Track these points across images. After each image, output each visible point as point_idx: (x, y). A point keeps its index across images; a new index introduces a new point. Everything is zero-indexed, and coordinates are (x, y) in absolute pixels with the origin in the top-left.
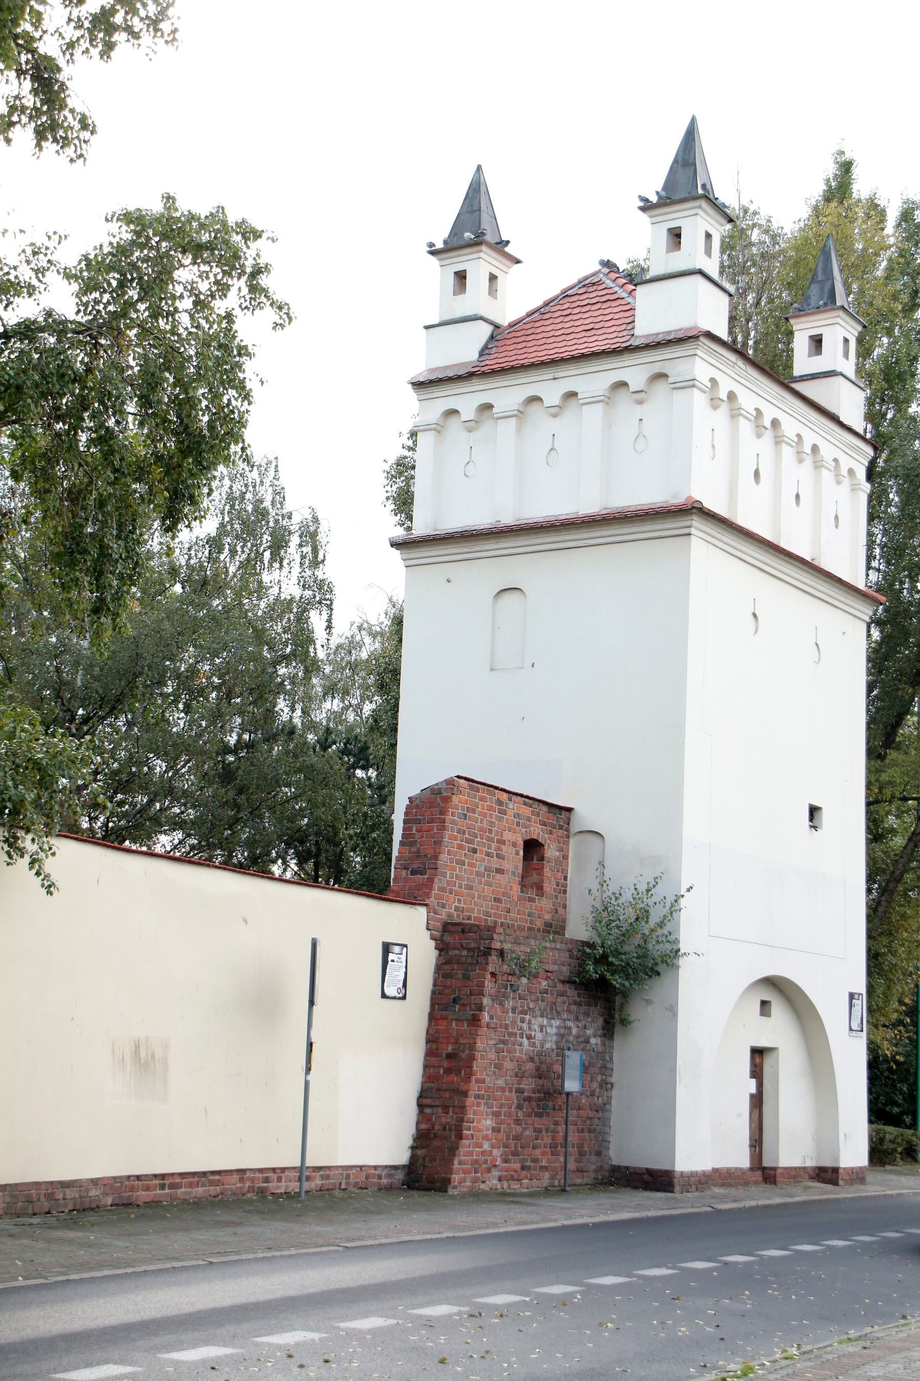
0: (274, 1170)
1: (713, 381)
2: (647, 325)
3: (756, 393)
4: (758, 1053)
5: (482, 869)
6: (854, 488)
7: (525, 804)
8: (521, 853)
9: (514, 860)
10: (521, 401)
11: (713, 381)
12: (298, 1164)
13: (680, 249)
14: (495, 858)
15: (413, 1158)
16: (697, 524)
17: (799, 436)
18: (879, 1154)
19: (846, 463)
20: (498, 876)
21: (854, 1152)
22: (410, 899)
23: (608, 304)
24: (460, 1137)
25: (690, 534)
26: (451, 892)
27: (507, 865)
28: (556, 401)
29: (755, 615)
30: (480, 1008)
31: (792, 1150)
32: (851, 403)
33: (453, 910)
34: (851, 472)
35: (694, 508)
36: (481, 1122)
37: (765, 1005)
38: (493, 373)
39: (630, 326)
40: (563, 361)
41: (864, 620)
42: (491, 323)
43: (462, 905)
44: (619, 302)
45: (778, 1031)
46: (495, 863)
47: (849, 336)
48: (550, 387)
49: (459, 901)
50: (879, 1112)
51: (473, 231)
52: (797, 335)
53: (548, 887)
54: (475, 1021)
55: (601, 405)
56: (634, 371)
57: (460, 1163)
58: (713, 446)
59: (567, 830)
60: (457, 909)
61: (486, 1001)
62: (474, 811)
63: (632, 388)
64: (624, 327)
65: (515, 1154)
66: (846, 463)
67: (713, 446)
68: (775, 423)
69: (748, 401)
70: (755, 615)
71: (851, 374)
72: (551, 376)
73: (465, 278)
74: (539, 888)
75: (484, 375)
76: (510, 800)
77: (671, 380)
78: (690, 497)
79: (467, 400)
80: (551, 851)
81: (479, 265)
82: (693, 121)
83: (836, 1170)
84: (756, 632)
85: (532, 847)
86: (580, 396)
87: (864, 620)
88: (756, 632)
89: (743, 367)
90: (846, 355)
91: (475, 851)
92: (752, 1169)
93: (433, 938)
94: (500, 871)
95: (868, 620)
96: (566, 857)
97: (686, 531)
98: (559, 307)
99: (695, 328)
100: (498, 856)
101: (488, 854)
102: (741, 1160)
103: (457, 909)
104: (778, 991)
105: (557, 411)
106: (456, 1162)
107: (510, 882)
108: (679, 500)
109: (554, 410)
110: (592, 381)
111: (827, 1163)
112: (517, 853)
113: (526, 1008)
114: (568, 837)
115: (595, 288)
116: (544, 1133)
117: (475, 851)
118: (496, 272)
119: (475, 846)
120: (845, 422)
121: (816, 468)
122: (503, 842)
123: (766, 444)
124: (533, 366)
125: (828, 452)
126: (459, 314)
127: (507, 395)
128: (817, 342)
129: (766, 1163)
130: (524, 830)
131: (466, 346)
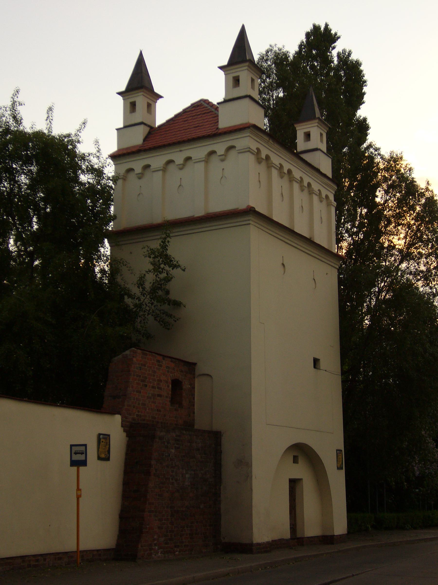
0: (41, 555)
1: (258, 149)
3: (279, 157)
5: (150, 395)
6: (329, 204)
7: (172, 361)
8: (170, 386)
9: (166, 390)
10: (164, 163)
11: (258, 149)
13: (302, 479)
14: (157, 389)
15: (118, 544)
16: (251, 219)
17: (301, 178)
19: (324, 193)
20: (159, 398)
21: (340, 526)
22: (112, 412)
23: (206, 114)
25: (250, 224)
26: (134, 407)
29: (283, 265)
31: (311, 528)
32: (325, 165)
33: (135, 416)
34: (327, 197)
35: (251, 210)
39: (216, 124)
41: (336, 268)
42: (149, 126)
43: (140, 414)
44: (211, 113)
45: (300, 471)
47: (322, 132)
48: (178, 156)
49: (138, 412)
50: (351, 507)
51: (140, 85)
52: (298, 132)
55: (203, 163)
56: (220, 146)
57: (142, 547)
58: (260, 181)
59: (194, 374)
60: (137, 415)
61: (153, 462)
62: (145, 365)
63: (219, 153)
64: (213, 125)
67: (260, 181)
68: (289, 171)
69: (276, 160)
70: (283, 265)
71: (325, 150)
72: (179, 150)
73: (135, 105)
76: (164, 359)
77: (237, 149)
78: (248, 206)
79: (137, 165)
80: (186, 386)
81: (141, 100)
82: (243, 27)
83: (333, 536)
84: (284, 273)
85: (176, 384)
86: (193, 159)
87: (336, 268)
88: (284, 273)
89: (273, 143)
90: (322, 141)
91: (146, 386)
92: (291, 539)
93: (124, 431)
94: (160, 396)
95: (338, 267)
96: (194, 388)
97: (248, 222)
98: (182, 117)
99: (248, 123)
100: (159, 388)
101: (153, 387)
102: (287, 535)
103: (137, 415)
104: (301, 452)
105: (182, 167)
106: (140, 546)
108: (242, 206)
109: (181, 166)
110: (198, 151)
111: (329, 533)
112: (168, 386)
113: (174, 465)
114: (194, 378)
115: (199, 108)
116: (186, 528)
117: (146, 386)
118: (150, 102)
119: (146, 384)
120: (323, 172)
121: (310, 194)
122: (161, 381)
123: (285, 182)
125: (316, 186)
126: (133, 122)
127: (157, 160)
128: (308, 136)
129: (299, 535)
130: (171, 375)
131: (137, 137)
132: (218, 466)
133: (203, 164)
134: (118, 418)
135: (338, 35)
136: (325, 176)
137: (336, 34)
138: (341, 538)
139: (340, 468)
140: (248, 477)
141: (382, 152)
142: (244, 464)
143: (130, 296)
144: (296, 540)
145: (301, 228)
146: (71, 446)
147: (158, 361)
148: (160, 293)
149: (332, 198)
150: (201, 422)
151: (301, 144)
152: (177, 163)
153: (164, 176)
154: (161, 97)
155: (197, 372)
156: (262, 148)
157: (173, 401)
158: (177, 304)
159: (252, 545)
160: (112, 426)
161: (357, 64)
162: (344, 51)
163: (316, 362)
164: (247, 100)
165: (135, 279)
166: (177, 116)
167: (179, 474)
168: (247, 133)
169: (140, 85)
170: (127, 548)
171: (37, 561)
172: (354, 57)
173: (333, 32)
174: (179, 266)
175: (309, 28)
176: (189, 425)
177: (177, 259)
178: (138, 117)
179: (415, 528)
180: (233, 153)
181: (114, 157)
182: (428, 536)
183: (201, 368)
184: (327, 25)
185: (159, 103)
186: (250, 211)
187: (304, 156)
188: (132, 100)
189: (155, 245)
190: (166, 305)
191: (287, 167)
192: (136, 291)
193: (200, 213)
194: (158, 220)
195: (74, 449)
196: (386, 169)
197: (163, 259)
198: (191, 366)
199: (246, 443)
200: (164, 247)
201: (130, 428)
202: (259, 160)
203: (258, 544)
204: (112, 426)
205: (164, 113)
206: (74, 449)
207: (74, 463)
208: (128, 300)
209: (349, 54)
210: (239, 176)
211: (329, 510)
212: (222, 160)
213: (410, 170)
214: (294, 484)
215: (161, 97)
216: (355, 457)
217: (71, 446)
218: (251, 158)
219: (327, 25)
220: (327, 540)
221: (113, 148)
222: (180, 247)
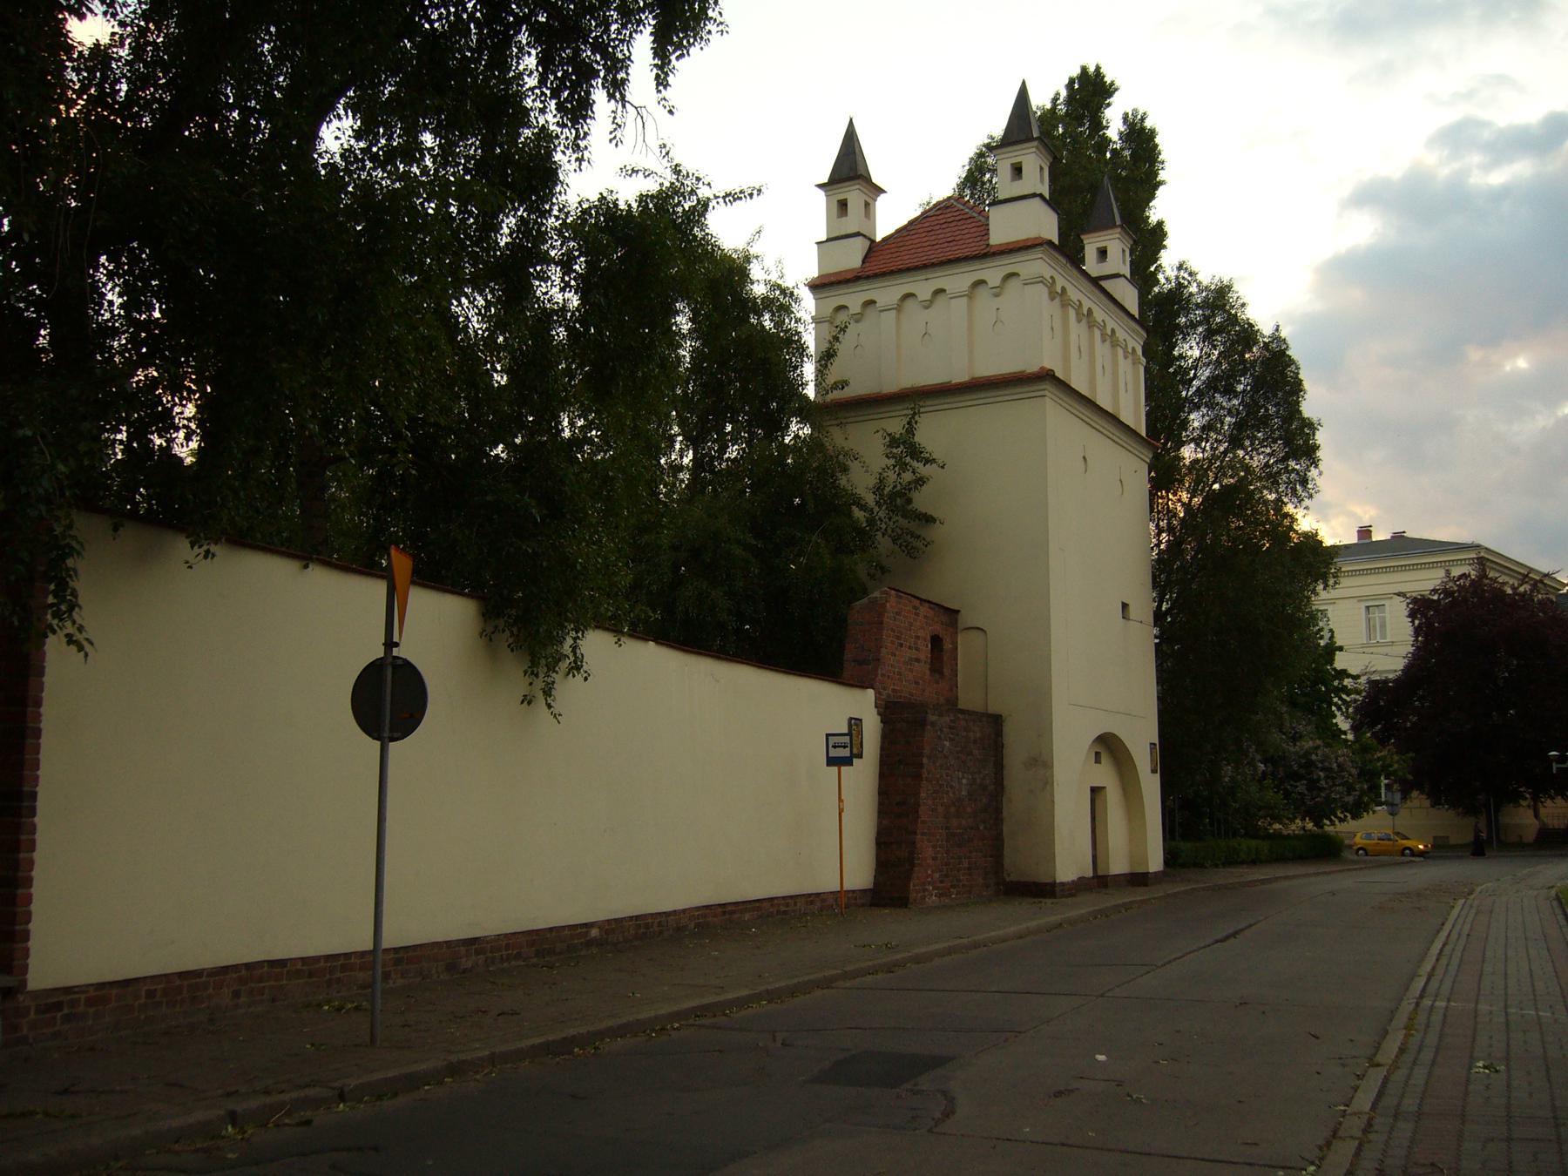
2: (997, 237)
4: (1095, 791)
12: (369, 946)
16: (1048, 389)
18: (1171, 858)
22: (862, 685)
24: (913, 865)
27: (922, 657)
28: (928, 296)
30: (921, 765)
31: (1118, 865)
36: (927, 850)
37: (1097, 754)
38: (876, 276)
40: (933, 265)
45: (1104, 775)
46: (914, 653)
48: (922, 286)
51: (850, 172)
53: (946, 671)
54: (918, 777)
56: (992, 273)
61: (925, 760)
65: (947, 876)
66: (1131, 343)
74: (941, 673)
75: (868, 277)
79: (854, 299)
80: (947, 646)
81: (854, 195)
83: (1146, 874)
85: (936, 641)
94: (918, 660)
104: (1109, 746)
105: (928, 305)
107: (924, 668)
108: (1033, 368)
110: (957, 280)
111: (1141, 870)
124: (908, 270)
127: (887, 293)
128: (1103, 253)
131: (851, 257)
132: (999, 766)
133: (965, 299)
134: (870, 694)
135: (1117, 84)
136: (1132, 317)
137: (1112, 84)
138: (1158, 878)
139: (1154, 771)
140: (1047, 783)
141: (1199, 277)
142: (1041, 763)
143: (863, 507)
144: (1100, 882)
145: (1104, 401)
146: (828, 735)
147: (915, 608)
148: (898, 500)
149: (1139, 352)
150: (969, 698)
151: (1091, 265)
152: (921, 298)
153: (898, 319)
154: (883, 191)
155: (960, 626)
156: (1057, 276)
157: (933, 670)
158: (929, 519)
159: (1053, 884)
160: (862, 704)
161: (1152, 134)
162: (1135, 111)
163: (1125, 606)
164: (1037, 200)
165: (872, 481)
166: (911, 223)
167: (946, 780)
168: (1038, 253)
169: (850, 172)
170: (892, 885)
171: (787, 905)
172: (1148, 124)
173: (1108, 80)
174: (934, 461)
175: (1075, 72)
176: (952, 703)
177: (929, 449)
178: (851, 223)
179: (1217, 866)
180: (1013, 282)
181: (816, 286)
182: (1291, 874)
183: (966, 619)
184: (1098, 68)
185: (881, 203)
186: (1046, 376)
187: (1103, 283)
188: (841, 197)
189: (896, 426)
190: (909, 519)
191: (1087, 304)
192: (870, 499)
193: (960, 377)
194: (890, 387)
195: (832, 740)
196: (1205, 304)
197: (907, 449)
198: (953, 613)
199: (1043, 730)
200: (910, 429)
201: (889, 711)
202: (1052, 295)
203: (1062, 884)
204: (862, 704)
205: (890, 217)
206: (832, 740)
207: (831, 761)
208: (858, 514)
209: (1143, 119)
210: (1017, 318)
211: (1137, 838)
212: (997, 295)
213: (1243, 305)
214: (1095, 791)
215: (883, 191)
216: (1173, 754)
217: (828, 735)
218: (1042, 291)
219: (1098, 68)
220: (1138, 879)
221: (813, 272)
222: (934, 431)
